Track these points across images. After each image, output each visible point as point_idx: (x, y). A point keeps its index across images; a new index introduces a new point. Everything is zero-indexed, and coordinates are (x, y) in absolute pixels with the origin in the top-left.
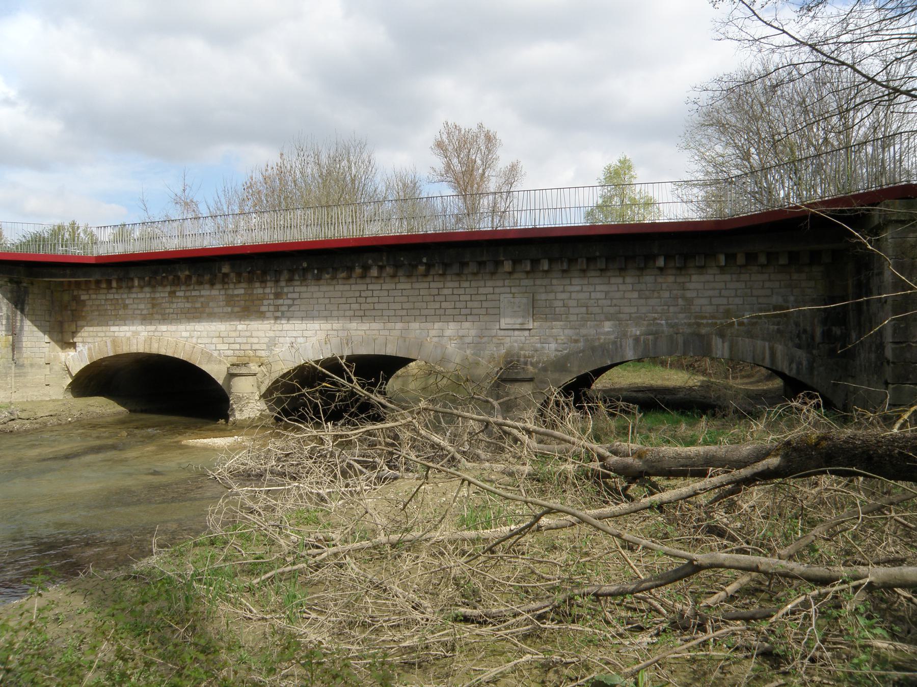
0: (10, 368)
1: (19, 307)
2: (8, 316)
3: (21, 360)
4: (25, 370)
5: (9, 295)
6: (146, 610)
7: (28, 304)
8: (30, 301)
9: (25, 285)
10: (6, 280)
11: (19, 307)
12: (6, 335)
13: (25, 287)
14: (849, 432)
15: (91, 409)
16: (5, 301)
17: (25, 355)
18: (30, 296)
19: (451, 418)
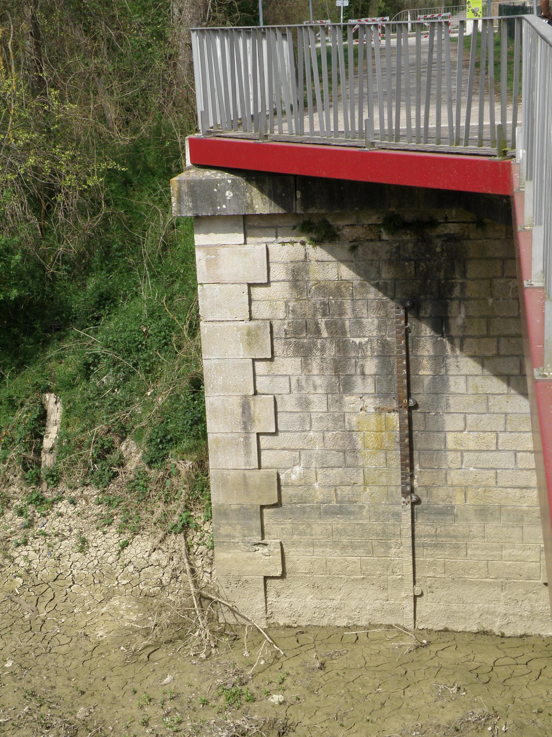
0: (397, 515)
1: (428, 310)
2: (384, 344)
3: (441, 493)
4: (460, 527)
5: (386, 274)
6: (13, 489)
7: (463, 299)
8: (472, 288)
9: (452, 229)
10: (374, 219)
11: (428, 310)
12: (379, 410)
13: (450, 238)
14: (492, 353)
15: (440, 553)
16: (373, 294)
17: (455, 477)
18: (473, 270)
19: (130, 356)
